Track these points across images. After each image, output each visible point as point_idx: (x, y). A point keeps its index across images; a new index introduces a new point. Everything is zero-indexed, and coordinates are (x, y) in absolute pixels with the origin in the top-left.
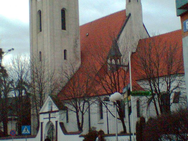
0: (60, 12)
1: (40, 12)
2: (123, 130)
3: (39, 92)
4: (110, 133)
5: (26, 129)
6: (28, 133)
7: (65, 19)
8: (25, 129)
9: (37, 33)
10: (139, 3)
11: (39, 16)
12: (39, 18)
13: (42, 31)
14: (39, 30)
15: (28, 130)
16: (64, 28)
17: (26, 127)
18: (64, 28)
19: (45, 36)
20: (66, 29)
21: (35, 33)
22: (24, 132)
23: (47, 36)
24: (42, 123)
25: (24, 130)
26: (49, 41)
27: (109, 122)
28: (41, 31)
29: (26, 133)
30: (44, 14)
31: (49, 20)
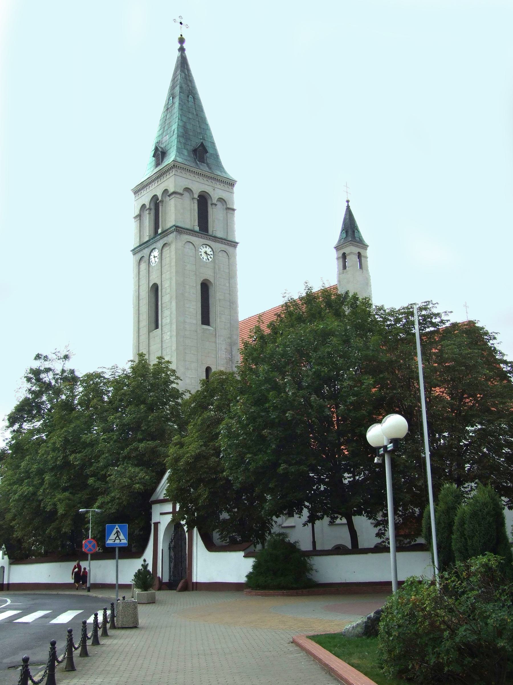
0: (199, 287)
1: (155, 289)
2: (194, 580)
3: (151, 433)
4: (318, 548)
5: (117, 532)
6: (123, 541)
7: (166, 514)
8: (115, 531)
9: (149, 332)
10: (364, 271)
11: (153, 296)
12: (153, 300)
13: (165, 188)
14: (153, 326)
15: (122, 537)
16: (206, 320)
17: (117, 527)
18: (206, 320)
19: (166, 337)
20: (211, 324)
21: (144, 331)
22: (111, 540)
23: (171, 337)
24: (156, 524)
25: (113, 536)
26: (174, 348)
27: (198, 571)
28: (157, 327)
29: (117, 541)
30: (164, 290)
31: (174, 304)
